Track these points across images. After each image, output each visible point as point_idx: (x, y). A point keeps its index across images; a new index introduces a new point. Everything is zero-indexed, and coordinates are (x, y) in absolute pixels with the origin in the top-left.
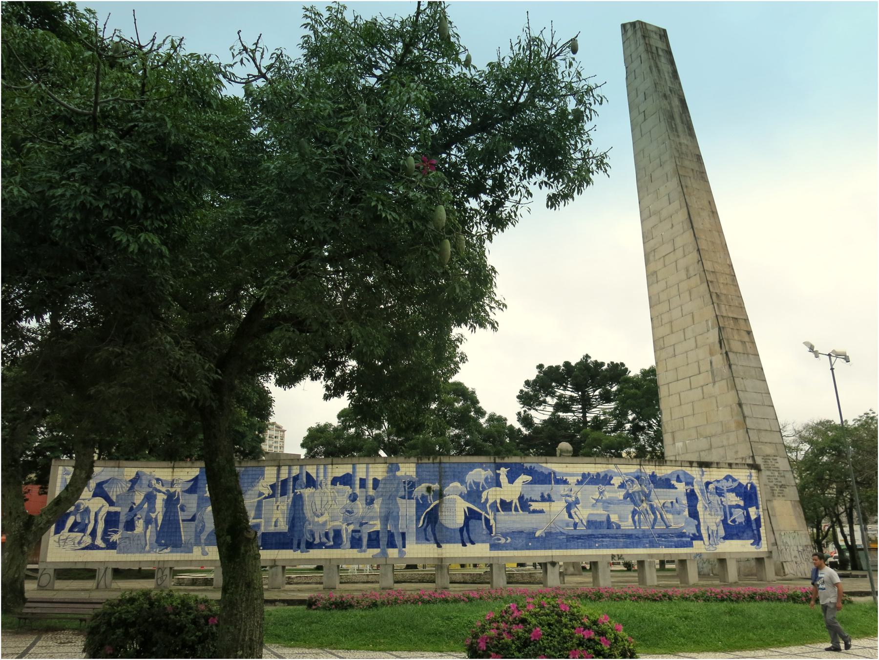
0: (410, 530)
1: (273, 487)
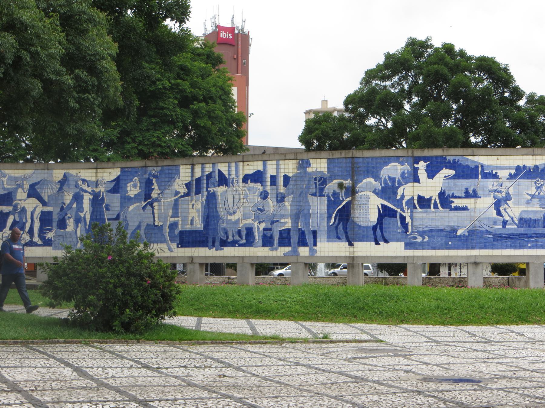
0: (321, 228)
1: (188, 185)
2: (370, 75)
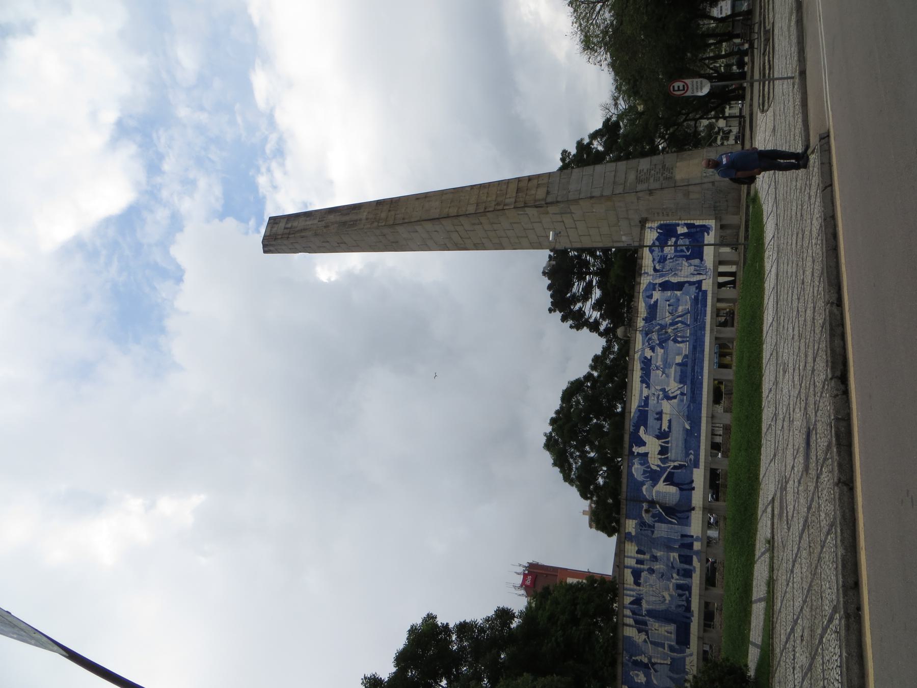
1: (640, 631)
2: (567, 478)
